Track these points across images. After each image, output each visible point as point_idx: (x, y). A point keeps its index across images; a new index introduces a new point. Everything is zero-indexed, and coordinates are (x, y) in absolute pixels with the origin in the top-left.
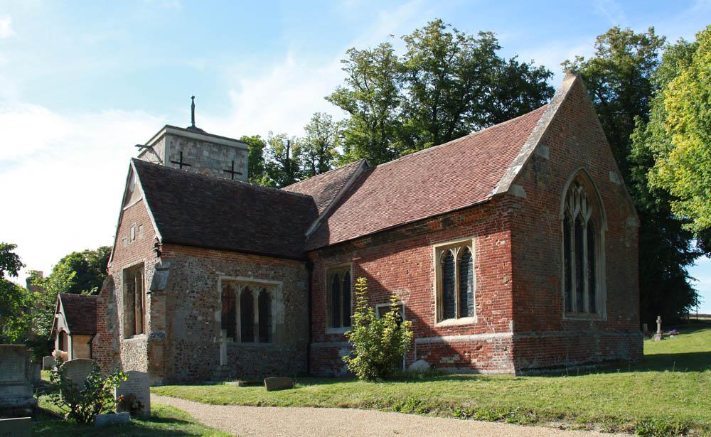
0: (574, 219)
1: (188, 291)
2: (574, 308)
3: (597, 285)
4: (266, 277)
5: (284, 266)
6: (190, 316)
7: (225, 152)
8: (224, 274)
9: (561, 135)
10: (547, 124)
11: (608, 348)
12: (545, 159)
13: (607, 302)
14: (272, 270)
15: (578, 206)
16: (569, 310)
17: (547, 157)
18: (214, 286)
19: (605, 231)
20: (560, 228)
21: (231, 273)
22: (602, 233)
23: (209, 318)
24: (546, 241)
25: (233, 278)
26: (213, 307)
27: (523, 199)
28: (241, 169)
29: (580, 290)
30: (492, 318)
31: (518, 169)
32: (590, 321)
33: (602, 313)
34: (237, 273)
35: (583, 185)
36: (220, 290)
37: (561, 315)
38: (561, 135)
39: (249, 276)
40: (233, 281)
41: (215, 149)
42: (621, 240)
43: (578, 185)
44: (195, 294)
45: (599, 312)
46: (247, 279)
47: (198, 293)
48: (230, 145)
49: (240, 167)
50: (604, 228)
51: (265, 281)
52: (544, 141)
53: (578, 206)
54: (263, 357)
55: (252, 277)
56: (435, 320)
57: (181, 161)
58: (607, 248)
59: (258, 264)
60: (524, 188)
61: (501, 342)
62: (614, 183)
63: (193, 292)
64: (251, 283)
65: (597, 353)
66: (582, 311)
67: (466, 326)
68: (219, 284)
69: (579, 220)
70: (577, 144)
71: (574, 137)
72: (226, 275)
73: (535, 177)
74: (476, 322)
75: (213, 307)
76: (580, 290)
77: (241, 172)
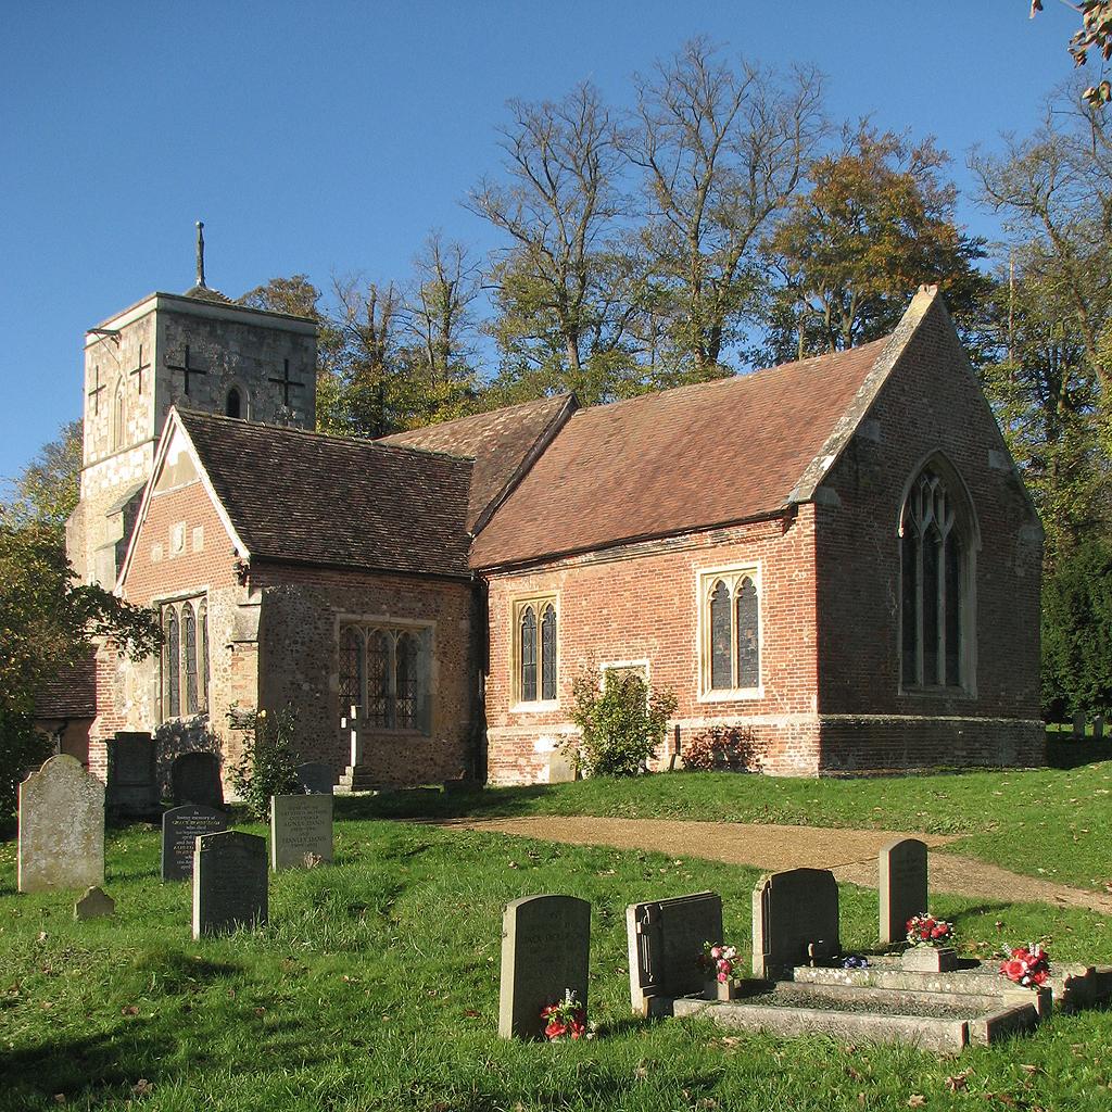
0: (922, 534)
1: (287, 642)
2: (920, 678)
3: (963, 641)
4: (410, 613)
5: (439, 593)
6: (292, 684)
7: (270, 341)
8: (343, 610)
9: (902, 399)
10: (879, 385)
11: (977, 745)
12: (873, 442)
13: (978, 669)
14: (420, 600)
15: (930, 511)
16: (910, 678)
17: (877, 439)
18: (329, 631)
19: (978, 552)
20: (897, 550)
21: (354, 608)
22: (972, 555)
23: (321, 687)
24: (871, 572)
25: (359, 617)
26: (326, 667)
27: (836, 508)
28: (303, 375)
29: (931, 646)
30: (785, 691)
31: (829, 461)
32: (946, 701)
33: (968, 686)
34: (364, 608)
35: (940, 476)
36: (337, 637)
37: (896, 688)
38: (902, 399)
39: (383, 613)
40: (357, 622)
41: (252, 338)
42: (1009, 564)
43: (931, 476)
44: (299, 647)
45: (964, 685)
46: (381, 618)
47: (303, 644)
48: (280, 326)
49: (302, 371)
50: (975, 546)
51: (408, 621)
52: (872, 413)
53: (930, 511)
54: (404, 753)
55: (388, 615)
56: (699, 691)
57: (187, 366)
58: (979, 580)
59: (398, 592)
60: (837, 491)
61: (798, 727)
62: (997, 470)
63: (296, 642)
64: (384, 624)
65: (957, 753)
66: (935, 683)
67: (747, 701)
68: (337, 627)
69: (931, 533)
70: (931, 411)
71: (925, 400)
72: (348, 612)
73: (857, 472)
74: (762, 696)
75: (326, 667)
76: (931, 646)
77: (303, 382)
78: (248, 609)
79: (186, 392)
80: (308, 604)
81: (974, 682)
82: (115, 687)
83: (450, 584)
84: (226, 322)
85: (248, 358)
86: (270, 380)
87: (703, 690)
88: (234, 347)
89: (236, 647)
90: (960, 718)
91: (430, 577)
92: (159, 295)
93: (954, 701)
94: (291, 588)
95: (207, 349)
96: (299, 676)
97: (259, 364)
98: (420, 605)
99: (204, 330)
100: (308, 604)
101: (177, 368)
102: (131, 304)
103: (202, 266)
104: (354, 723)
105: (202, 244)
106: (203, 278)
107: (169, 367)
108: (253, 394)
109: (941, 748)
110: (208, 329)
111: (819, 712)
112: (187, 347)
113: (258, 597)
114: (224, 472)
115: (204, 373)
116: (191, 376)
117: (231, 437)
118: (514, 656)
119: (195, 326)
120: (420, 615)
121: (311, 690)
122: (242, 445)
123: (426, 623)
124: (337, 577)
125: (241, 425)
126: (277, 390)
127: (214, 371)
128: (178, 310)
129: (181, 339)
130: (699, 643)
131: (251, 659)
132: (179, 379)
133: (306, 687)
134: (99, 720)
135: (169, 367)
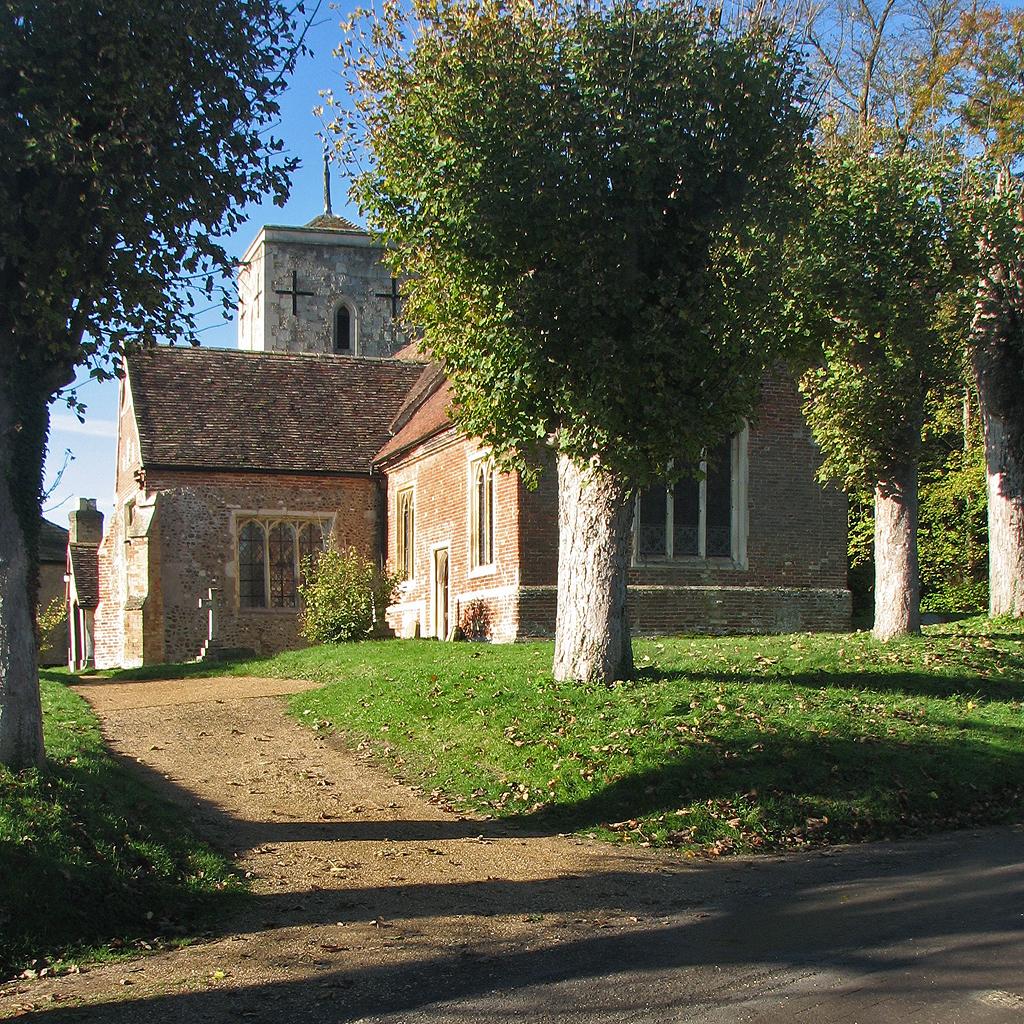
4: (310, 506)
5: (339, 487)
6: (189, 571)
11: (744, 614)
13: (749, 540)
18: (225, 526)
21: (250, 505)
25: (254, 512)
26: (222, 556)
33: (739, 556)
39: (281, 507)
40: (256, 516)
45: (735, 556)
47: (198, 537)
55: (285, 509)
68: (233, 522)
75: (222, 556)
78: (145, 509)
79: (294, 313)
80: (203, 503)
81: (744, 551)
82: (111, 578)
83: (350, 480)
84: (332, 247)
85: (356, 277)
86: (377, 295)
87: (472, 567)
88: (341, 268)
89: (132, 541)
90: (676, 588)
91: (326, 474)
92: (266, 228)
93: (713, 571)
94: (185, 490)
95: (313, 273)
96: (195, 565)
97: (366, 282)
98: (320, 499)
99: (311, 256)
100: (203, 503)
101: (284, 292)
102: (253, 237)
103: (328, 195)
104: (210, 604)
105: (328, 175)
106: (329, 205)
107: (277, 292)
108: (361, 310)
109: (690, 617)
110: (315, 253)
111: (521, 584)
112: (295, 272)
113: (153, 498)
114: (150, 393)
115: (312, 294)
116: (298, 298)
117: (170, 361)
118: (398, 541)
119: (302, 253)
120: (320, 508)
121: (208, 576)
122: (178, 369)
123: (327, 514)
124: (232, 478)
125: (185, 351)
126: (384, 304)
127: (321, 291)
128: (286, 240)
129: (289, 265)
130: (469, 525)
131: (143, 551)
132: (287, 302)
133: (202, 573)
134: (101, 606)
135: (277, 292)
